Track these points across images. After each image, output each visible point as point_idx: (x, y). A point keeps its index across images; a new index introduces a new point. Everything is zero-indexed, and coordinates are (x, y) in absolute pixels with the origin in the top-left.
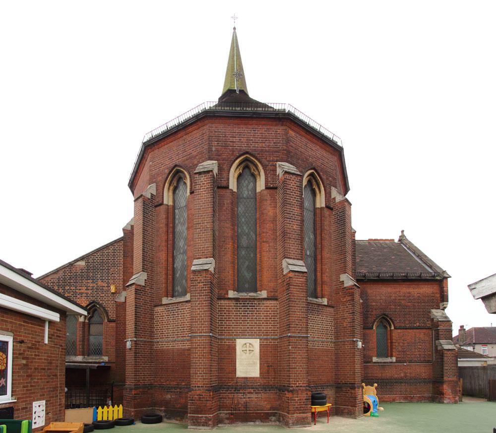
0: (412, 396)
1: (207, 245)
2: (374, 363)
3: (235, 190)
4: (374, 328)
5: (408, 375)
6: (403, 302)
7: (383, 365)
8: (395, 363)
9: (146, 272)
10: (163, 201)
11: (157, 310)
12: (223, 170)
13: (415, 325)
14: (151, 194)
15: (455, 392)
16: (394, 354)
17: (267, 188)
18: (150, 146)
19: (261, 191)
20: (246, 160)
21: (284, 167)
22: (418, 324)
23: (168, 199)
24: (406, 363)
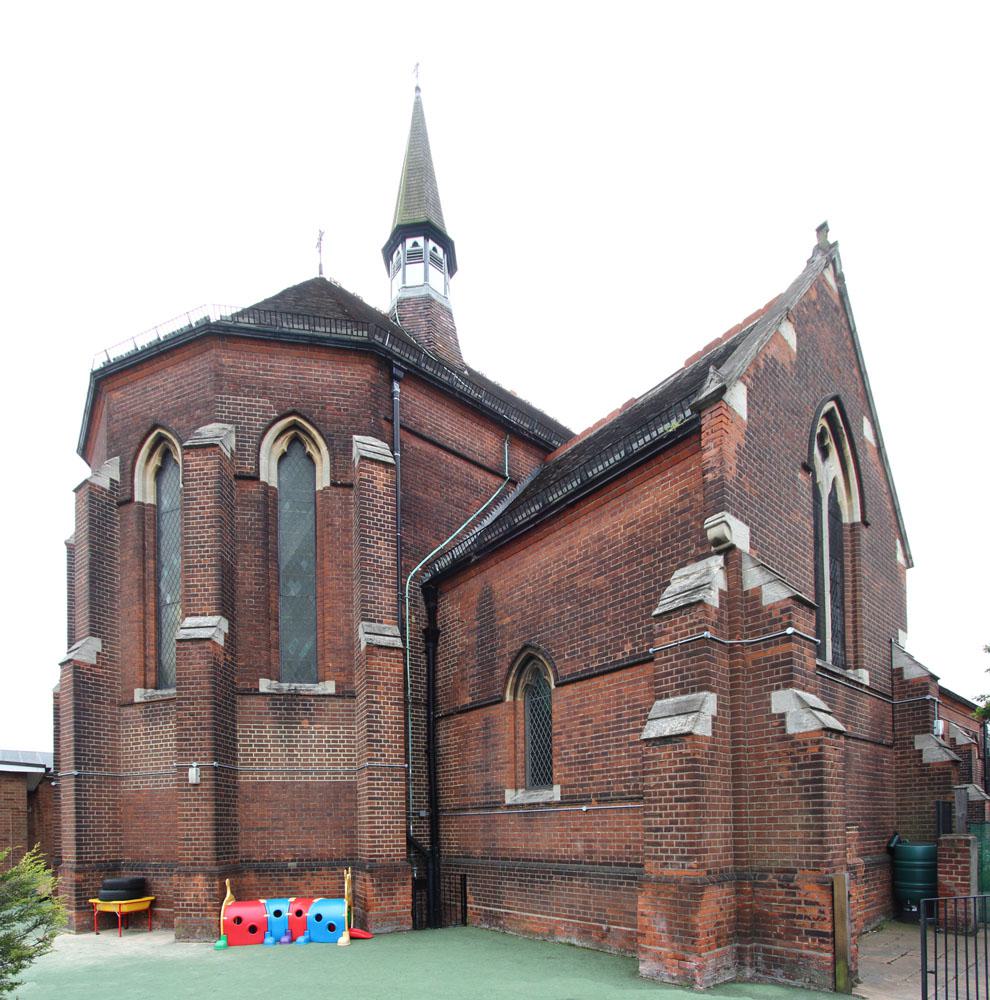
0: (604, 927)
1: (207, 582)
2: (509, 807)
3: (274, 483)
4: (508, 700)
5: (597, 846)
6: (580, 582)
7: (530, 812)
8: (559, 804)
9: (100, 637)
10: (133, 495)
11: (126, 714)
12: (250, 443)
13: (620, 656)
14: (111, 480)
15: (685, 935)
16: (556, 774)
17: (334, 484)
18: (105, 380)
19: (324, 489)
20: (294, 426)
21: (366, 445)
22: (628, 648)
23: (144, 490)
24: (588, 802)
